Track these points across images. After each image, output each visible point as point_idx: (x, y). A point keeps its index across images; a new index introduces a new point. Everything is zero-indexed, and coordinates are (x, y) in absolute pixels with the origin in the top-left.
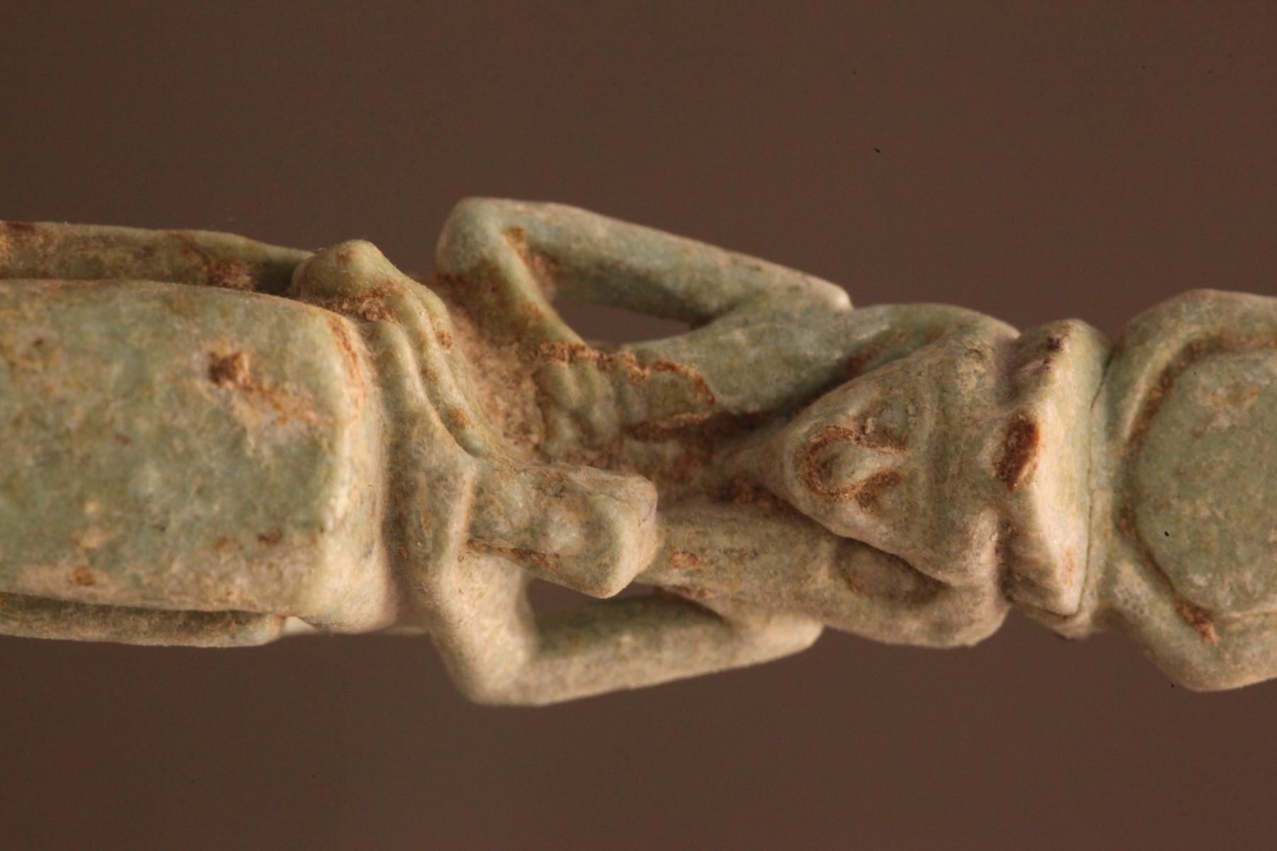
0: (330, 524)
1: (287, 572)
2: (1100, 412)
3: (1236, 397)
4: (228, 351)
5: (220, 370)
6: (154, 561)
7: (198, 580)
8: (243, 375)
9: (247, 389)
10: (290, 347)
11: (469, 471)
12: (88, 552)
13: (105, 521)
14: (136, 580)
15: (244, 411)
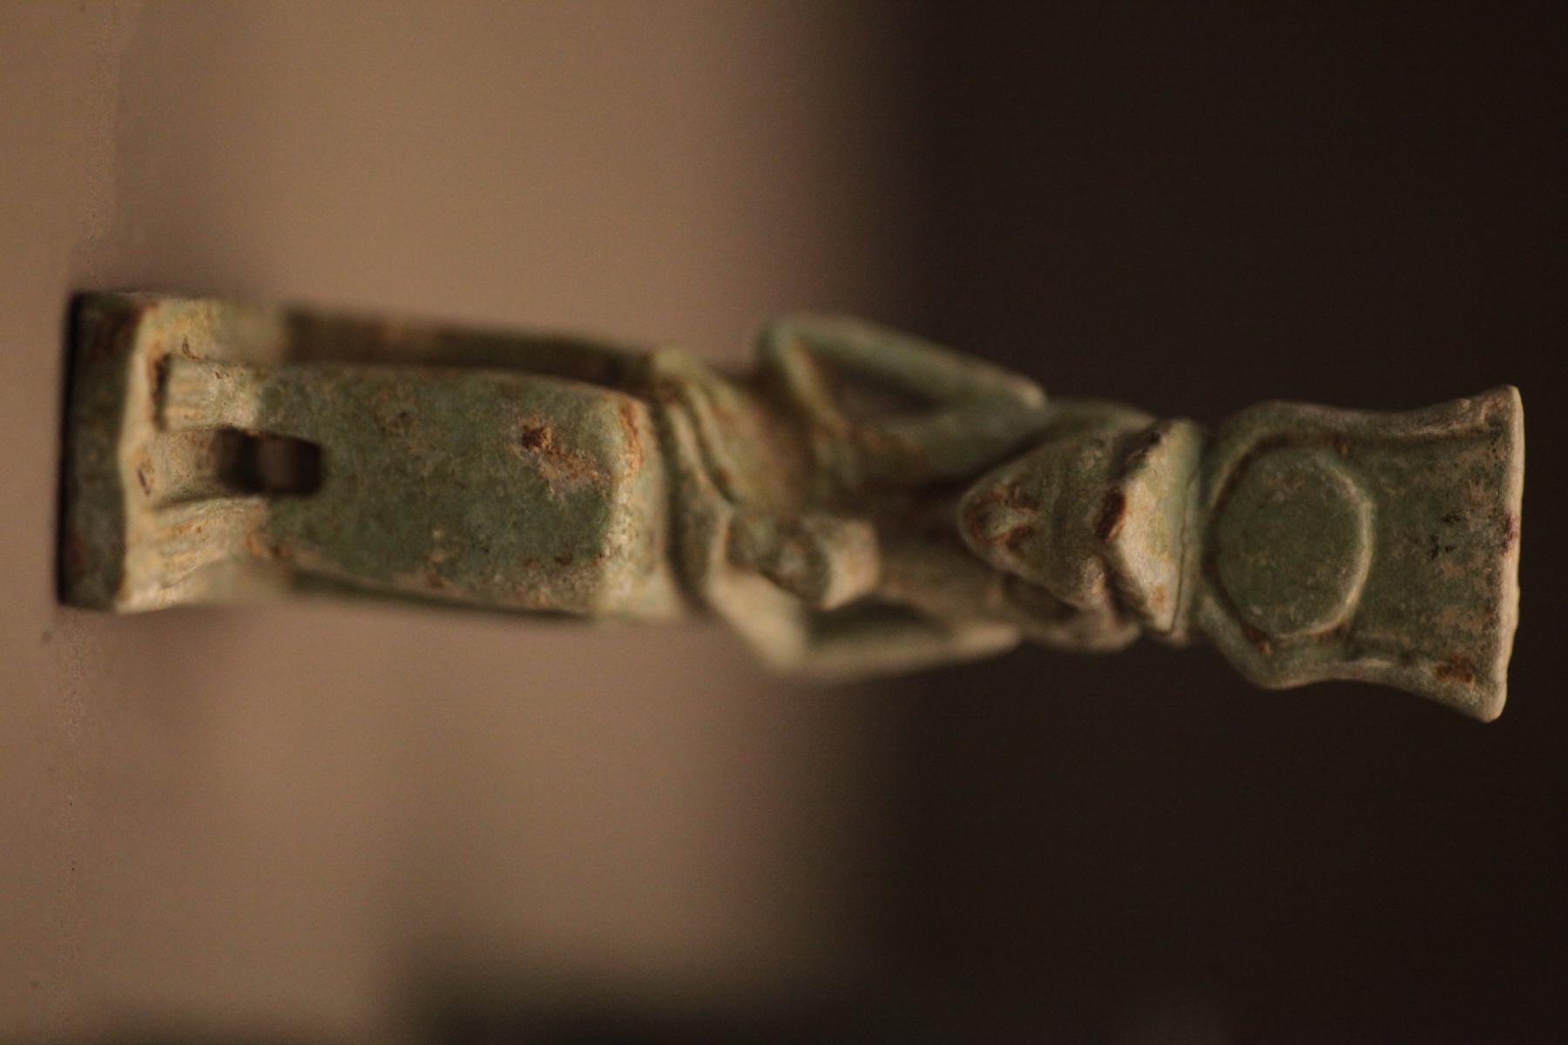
0: (607, 552)
1: (577, 584)
2: (1194, 487)
3: (1290, 479)
4: (538, 425)
5: (530, 438)
6: (482, 574)
7: (514, 587)
10: (582, 424)
11: (724, 514)
12: (436, 565)
13: (446, 544)
14: (472, 587)
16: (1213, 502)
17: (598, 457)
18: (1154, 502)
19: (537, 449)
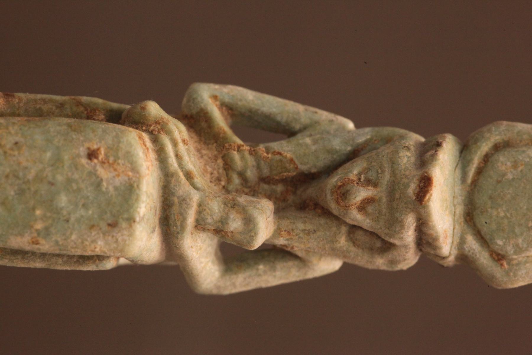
0: (138, 219)
1: (120, 239)
2: (458, 172)
3: (515, 166)
4: (95, 147)
5: (92, 155)
6: (64, 235)
7: (82, 242)
8: (101, 157)
9: (103, 163)
10: (121, 145)
11: (196, 197)
12: (37, 230)
13: (44, 218)
15: (102, 172)
16: (469, 181)
17: (131, 164)
18: (443, 181)
19: (96, 161)
